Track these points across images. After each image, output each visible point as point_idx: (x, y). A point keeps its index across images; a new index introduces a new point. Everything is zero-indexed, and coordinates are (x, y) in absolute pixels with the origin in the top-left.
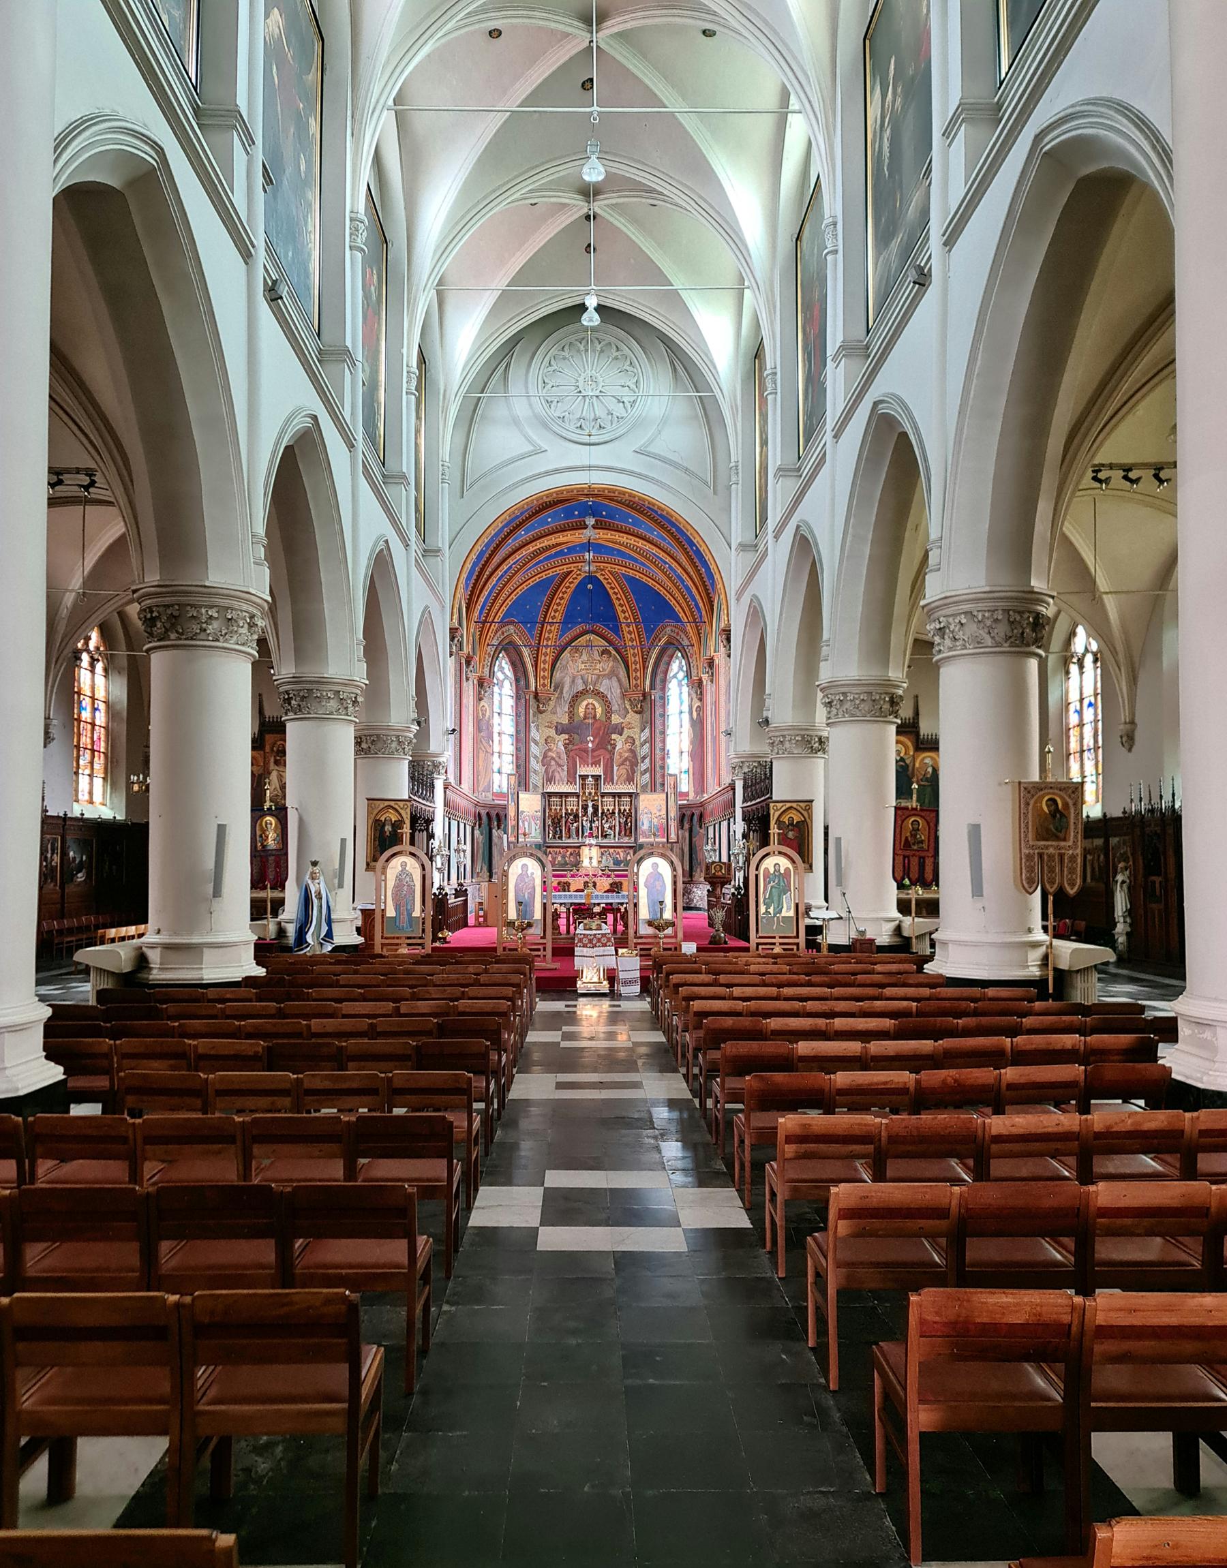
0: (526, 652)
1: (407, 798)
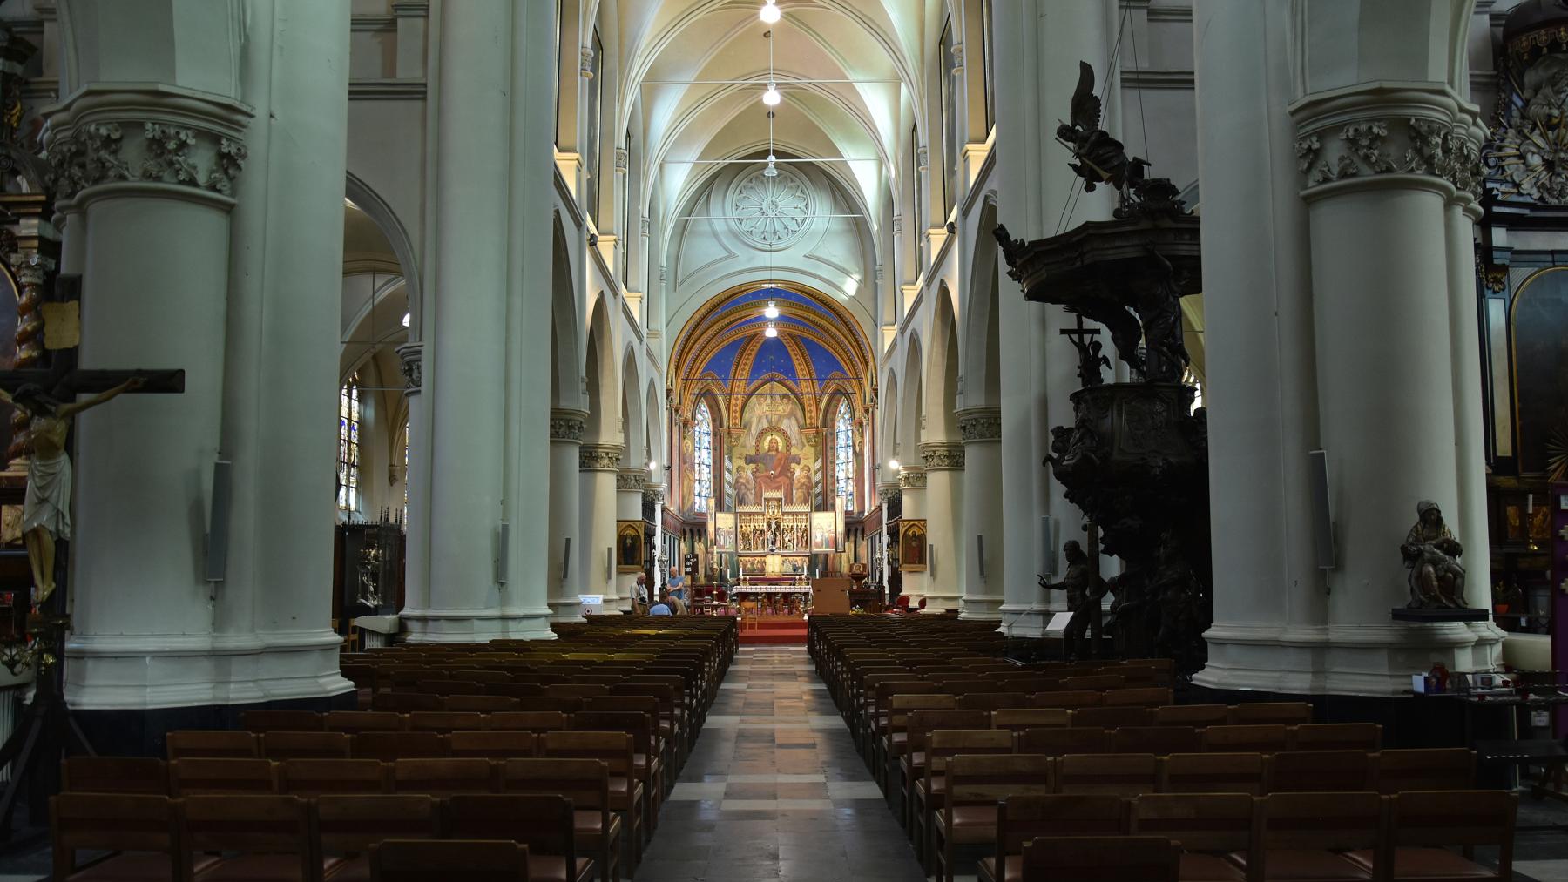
0: (720, 398)
1: (641, 519)
